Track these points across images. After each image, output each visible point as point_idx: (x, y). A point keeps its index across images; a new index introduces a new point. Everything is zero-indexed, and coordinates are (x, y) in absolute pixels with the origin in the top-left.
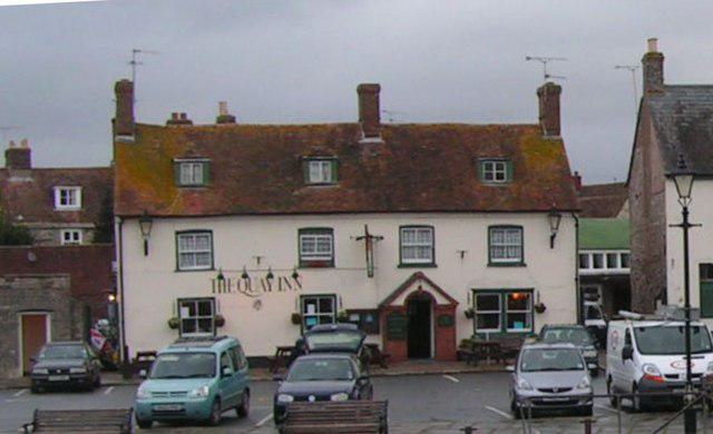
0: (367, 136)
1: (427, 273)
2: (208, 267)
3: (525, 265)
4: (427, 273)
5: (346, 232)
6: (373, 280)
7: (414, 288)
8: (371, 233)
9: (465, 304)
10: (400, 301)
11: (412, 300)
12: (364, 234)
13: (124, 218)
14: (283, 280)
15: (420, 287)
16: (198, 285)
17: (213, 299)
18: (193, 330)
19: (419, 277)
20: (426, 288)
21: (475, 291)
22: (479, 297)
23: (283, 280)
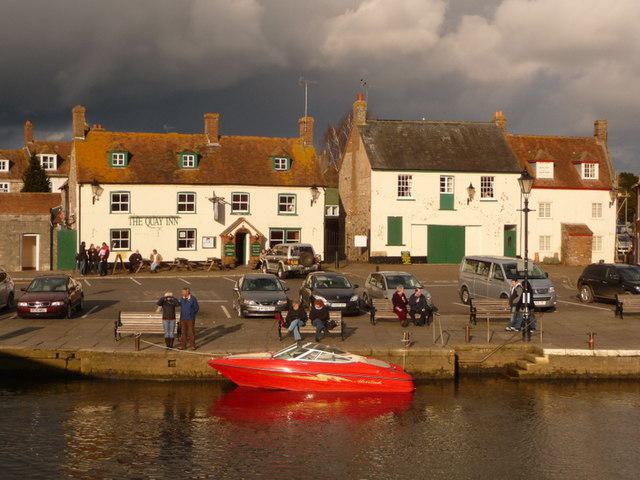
1: (246, 217)
5: (203, 193)
7: (240, 226)
9: (267, 235)
10: (233, 233)
13: (81, 184)
16: (120, 220)
18: (185, 247)
19: (241, 220)
20: (247, 226)
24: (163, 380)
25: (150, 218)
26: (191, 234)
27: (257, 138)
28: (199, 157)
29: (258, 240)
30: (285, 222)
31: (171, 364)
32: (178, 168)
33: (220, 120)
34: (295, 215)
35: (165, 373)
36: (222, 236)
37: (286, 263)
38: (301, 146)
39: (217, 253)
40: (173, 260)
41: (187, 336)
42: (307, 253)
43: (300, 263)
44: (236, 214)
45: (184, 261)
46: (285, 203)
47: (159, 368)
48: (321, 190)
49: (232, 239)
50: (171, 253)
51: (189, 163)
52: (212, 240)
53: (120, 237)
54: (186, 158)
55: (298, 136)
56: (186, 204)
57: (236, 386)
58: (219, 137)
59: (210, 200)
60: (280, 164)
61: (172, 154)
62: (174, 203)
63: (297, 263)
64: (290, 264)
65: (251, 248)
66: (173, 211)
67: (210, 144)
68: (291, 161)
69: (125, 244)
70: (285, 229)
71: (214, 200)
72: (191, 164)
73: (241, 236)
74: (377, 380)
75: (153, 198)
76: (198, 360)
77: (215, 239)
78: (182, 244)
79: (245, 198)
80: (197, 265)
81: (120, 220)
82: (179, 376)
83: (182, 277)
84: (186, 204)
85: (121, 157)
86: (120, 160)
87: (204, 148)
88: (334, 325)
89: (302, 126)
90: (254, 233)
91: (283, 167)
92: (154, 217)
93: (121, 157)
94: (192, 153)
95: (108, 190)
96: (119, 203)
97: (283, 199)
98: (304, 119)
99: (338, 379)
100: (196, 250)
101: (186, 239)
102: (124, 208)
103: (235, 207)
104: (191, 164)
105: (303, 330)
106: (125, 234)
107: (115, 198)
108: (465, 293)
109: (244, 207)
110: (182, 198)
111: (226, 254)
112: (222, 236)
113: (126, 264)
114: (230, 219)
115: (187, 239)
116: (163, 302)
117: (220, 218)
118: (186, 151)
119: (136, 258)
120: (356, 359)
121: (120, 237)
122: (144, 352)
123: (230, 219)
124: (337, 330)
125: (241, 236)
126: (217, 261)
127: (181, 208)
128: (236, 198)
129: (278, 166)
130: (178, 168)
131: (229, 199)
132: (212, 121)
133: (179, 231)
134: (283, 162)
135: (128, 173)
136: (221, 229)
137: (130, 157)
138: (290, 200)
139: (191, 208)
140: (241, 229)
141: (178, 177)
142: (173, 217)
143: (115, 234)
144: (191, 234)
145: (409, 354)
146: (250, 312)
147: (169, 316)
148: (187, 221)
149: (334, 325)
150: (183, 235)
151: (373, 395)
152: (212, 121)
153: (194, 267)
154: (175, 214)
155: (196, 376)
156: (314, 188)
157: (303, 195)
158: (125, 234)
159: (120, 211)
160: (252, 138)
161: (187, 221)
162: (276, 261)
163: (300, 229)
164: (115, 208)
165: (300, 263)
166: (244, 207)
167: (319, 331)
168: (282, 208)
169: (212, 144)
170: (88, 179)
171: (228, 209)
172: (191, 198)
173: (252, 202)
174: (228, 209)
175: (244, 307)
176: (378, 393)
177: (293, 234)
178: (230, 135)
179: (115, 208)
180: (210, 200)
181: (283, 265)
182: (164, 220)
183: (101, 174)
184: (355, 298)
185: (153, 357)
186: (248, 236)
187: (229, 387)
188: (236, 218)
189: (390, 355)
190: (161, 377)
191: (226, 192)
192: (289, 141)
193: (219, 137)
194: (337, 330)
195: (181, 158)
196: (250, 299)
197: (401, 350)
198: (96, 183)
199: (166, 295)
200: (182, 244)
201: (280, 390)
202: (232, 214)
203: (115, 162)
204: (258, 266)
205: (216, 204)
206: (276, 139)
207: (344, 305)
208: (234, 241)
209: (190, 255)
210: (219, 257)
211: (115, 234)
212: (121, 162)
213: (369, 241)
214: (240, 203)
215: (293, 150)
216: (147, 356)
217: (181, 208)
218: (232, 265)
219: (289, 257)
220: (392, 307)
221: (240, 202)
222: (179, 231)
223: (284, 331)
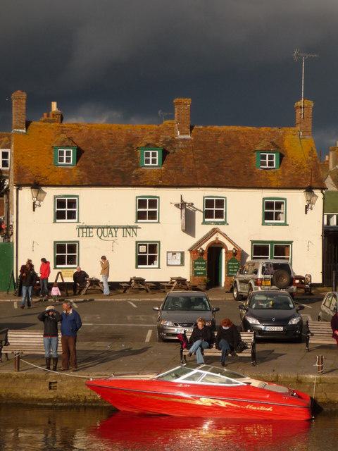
0: (181, 134)
1: (221, 228)
2: (157, 221)
3: (288, 225)
4: (221, 228)
5: (168, 198)
6: (47, 424)
7: (213, 239)
8: (185, 200)
9: (248, 250)
10: (204, 247)
11: (210, 248)
12: (179, 202)
13: (19, 186)
14: (114, 235)
15: (217, 238)
16: (66, 231)
17: (78, 242)
18: (64, 263)
19: (214, 231)
20: (221, 239)
21: (253, 242)
22: (139, 200)
23: (114, 235)
24: (50, 404)
25: (103, 228)
26: (153, 247)
27: (237, 128)
28: (165, 154)
29: (237, 255)
30: (272, 234)
31: (51, 386)
32: (138, 167)
33: (192, 105)
34: (285, 224)
35: (45, 396)
36: (190, 250)
37: (256, 284)
38: (296, 137)
39: (185, 273)
40: (169, 280)
41: (70, 360)
42: (281, 272)
43: (272, 284)
44: (267, 224)
45: (140, 281)
46: (272, 211)
47: (39, 391)
48: (318, 192)
49: (202, 254)
50: (124, 270)
51: (152, 160)
52: (179, 256)
53: (66, 252)
54: (148, 155)
55: (294, 126)
56: (147, 210)
57: (118, 410)
58: (192, 128)
59: (177, 205)
60: (267, 160)
61: (132, 149)
62: (132, 209)
63: (269, 283)
64: (261, 285)
65: (227, 266)
66: (131, 219)
67: (179, 136)
68: (281, 157)
69: (72, 260)
70: (272, 242)
71: (182, 205)
72: (154, 161)
73: (215, 250)
74: (267, 406)
75: (107, 205)
76: (75, 384)
77: (182, 254)
78: (141, 260)
79: (220, 203)
80: (157, 287)
81: (66, 231)
82: (62, 400)
83: (132, 300)
84: (147, 210)
85: (68, 153)
86: (67, 157)
87: (173, 142)
88: (244, 347)
89: (299, 112)
90: (230, 247)
91: (271, 164)
92: (108, 227)
93: (68, 153)
94: (156, 147)
95: (51, 193)
96: (65, 210)
97: (268, 205)
98: (300, 103)
99: (223, 404)
100: (159, 268)
101: (148, 254)
102: (72, 215)
103: (208, 214)
104: (154, 161)
105: (208, 353)
106: (72, 247)
107: (60, 203)
108: (60, 276)
109: (220, 214)
110: (141, 203)
111: (195, 273)
112: (190, 250)
113: (69, 284)
114: (202, 230)
115: (148, 254)
116: (43, 317)
117: (189, 228)
118: (148, 146)
119: (81, 277)
120: (256, 383)
121: (66, 252)
122: (24, 373)
123: (202, 230)
124: (247, 353)
125: (215, 250)
126: (181, 281)
127: (140, 216)
128: (209, 203)
129: (264, 164)
130: (138, 167)
131: (199, 205)
132: (183, 106)
133: (139, 244)
134: (271, 157)
135: (76, 173)
136: (190, 241)
137: (79, 153)
138: (279, 205)
139: (153, 215)
140: (213, 243)
141: (137, 177)
142: (130, 227)
143: (60, 247)
144: (153, 247)
145: (320, 381)
146: (168, 335)
147: (50, 333)
148: (148, 231)
149: (244, 347)
150: (143, 249)
151: (265, 422)
152: (183, 106)
153: (152, 288)
154: (132, 224)
155: (78, 401)
156: (309, 190)
157: (294, 199)
158: (72, 247)
159: (66, 220)
160: (231, 128)
161: (148, 231)
162: (246, 282)
163: (291, 242)
164: (60, 215)
165: (272, 284)
166: (220, 214)
167: (225, 354)
168: (267, 216)
169: (182, 137)
170: (28, 182)
171: (199, 216)
172: (153, 203)
173: (230, 209)
174: (199, 216)
175: (161, 329)
176: (271, 420)
177: (282, 249)
178: (205, 125)
179: (60, 215)
180: (177, 205)
181: (253, 286)
182: (120, 231)
183: (44, 174)
184: (294, 321)
185: (33, 378)
186: (224, 251)
187: (113, 412)
188: (209, 228)
189: (299, 382)
190: (40, 400)
191: (196, 197)
192: (281, 131)
193: (192, 128)
194: (247, 353)
195: (141, 154)
196: (168, 320)
197: (311, 376)
198: (36, 186)
199: (48, 309)
200: (141, 260)
201: (166, 415)
202: (204, 223)
203: (61, 160)
204: (232, 287)
205: (184, 211)
206: (263, 129)
207: (281, 329)
208: (205, 257)
209: (150, 274)
210: (184, 276)
211: (60, 247)
212: (68, 160)
213: (178, 252)
214: (215, 209)
215: (286, 144)
216: (26, 377)
217: (140, 216)
218: (202, 287)
219: (260, 276)
220: (331, 331)
221: (66, 209)
222: (139, 244)
223: (186, 353)
